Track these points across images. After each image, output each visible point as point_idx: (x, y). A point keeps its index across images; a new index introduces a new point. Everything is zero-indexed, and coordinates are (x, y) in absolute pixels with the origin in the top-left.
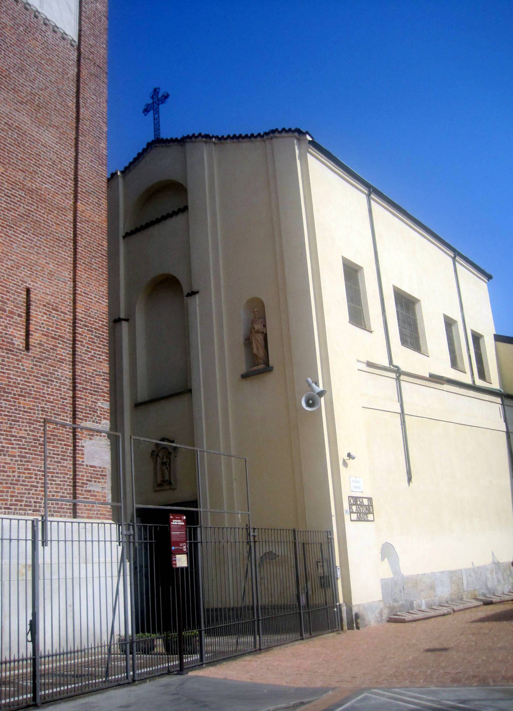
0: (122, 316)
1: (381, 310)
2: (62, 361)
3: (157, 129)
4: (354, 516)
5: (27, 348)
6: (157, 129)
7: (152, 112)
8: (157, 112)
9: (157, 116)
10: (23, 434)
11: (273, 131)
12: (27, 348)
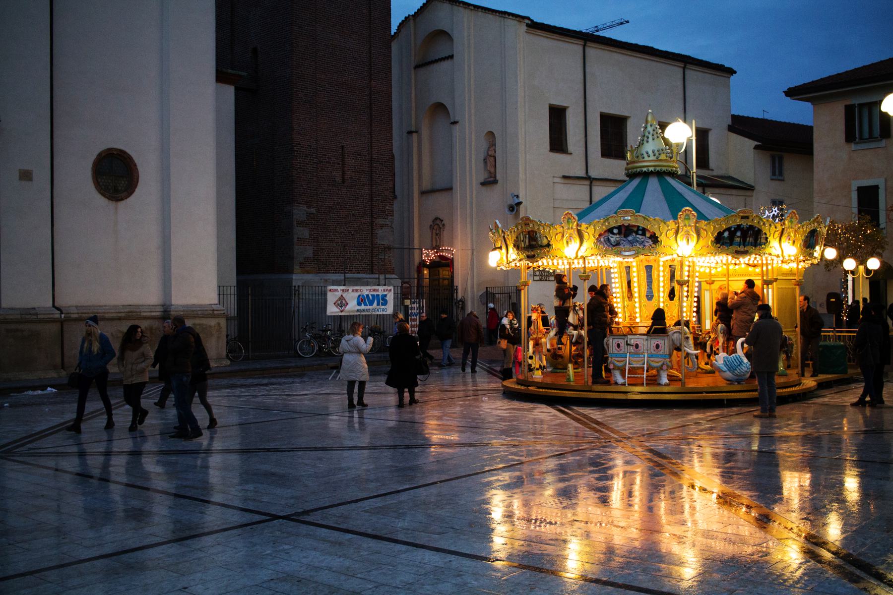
0: (413, 129)
2: (364, 185)
4: (537, 278)
5: (343, 182)
10: (342, 230)
11: (505, 13)
12: (343, 182)
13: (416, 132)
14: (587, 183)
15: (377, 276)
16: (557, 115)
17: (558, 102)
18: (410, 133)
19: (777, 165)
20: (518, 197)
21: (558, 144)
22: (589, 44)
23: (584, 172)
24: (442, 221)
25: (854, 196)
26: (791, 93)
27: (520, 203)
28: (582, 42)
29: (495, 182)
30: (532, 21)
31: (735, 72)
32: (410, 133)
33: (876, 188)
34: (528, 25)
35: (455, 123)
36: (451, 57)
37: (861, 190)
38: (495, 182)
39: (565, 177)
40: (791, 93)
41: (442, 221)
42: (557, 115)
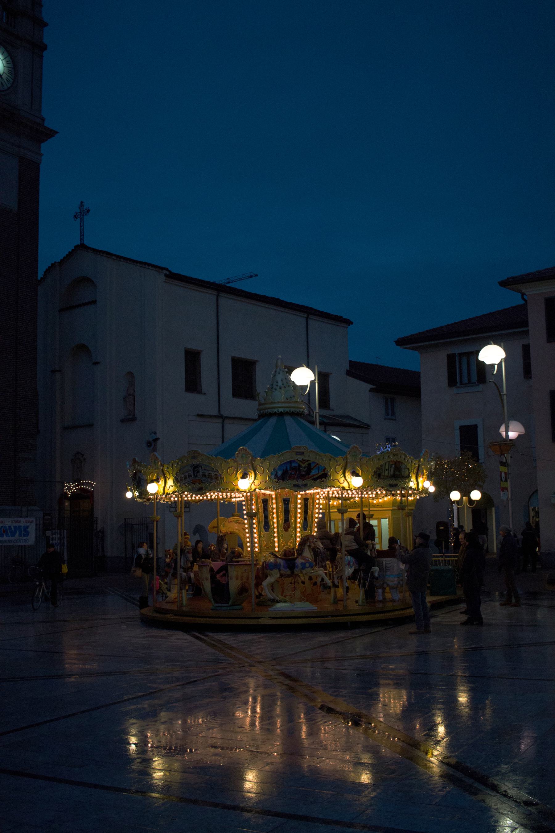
1: (216, 375)
3: (82, 239)
6: (82, 239)
7: (79, 219)
8: (82, 220)
9: (82, 224)
13: (60, 371)
14: (220, 421)
15: (19, 508)
16: (192, 358)
17: (194, 346)
18: (54, 371)
19: (389, 403)
20: (155, 433)
21: (193, 384)
22: (221, 294)
23: (217, 411)
24: (83, 455)
25: (457, 433)
26: (401, 342)
27: (157, 439)
28: (215, 293)
29: (134, 419)
30: (170, 272)
31: (352, 323)
32: (54, 371)
33: (475, 427)
34: (166, 276)
35: (97, 363)
36: (94, 302)
37: (462, 428)
38: (134, 419)
39: (199, 415)
40: (401, 342)
41: (83, 455)
42: (192, 358)
